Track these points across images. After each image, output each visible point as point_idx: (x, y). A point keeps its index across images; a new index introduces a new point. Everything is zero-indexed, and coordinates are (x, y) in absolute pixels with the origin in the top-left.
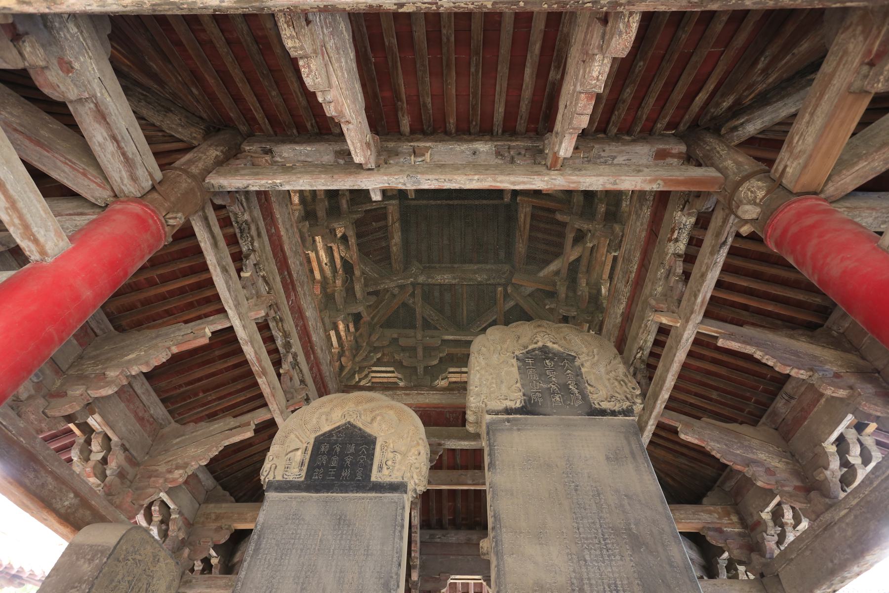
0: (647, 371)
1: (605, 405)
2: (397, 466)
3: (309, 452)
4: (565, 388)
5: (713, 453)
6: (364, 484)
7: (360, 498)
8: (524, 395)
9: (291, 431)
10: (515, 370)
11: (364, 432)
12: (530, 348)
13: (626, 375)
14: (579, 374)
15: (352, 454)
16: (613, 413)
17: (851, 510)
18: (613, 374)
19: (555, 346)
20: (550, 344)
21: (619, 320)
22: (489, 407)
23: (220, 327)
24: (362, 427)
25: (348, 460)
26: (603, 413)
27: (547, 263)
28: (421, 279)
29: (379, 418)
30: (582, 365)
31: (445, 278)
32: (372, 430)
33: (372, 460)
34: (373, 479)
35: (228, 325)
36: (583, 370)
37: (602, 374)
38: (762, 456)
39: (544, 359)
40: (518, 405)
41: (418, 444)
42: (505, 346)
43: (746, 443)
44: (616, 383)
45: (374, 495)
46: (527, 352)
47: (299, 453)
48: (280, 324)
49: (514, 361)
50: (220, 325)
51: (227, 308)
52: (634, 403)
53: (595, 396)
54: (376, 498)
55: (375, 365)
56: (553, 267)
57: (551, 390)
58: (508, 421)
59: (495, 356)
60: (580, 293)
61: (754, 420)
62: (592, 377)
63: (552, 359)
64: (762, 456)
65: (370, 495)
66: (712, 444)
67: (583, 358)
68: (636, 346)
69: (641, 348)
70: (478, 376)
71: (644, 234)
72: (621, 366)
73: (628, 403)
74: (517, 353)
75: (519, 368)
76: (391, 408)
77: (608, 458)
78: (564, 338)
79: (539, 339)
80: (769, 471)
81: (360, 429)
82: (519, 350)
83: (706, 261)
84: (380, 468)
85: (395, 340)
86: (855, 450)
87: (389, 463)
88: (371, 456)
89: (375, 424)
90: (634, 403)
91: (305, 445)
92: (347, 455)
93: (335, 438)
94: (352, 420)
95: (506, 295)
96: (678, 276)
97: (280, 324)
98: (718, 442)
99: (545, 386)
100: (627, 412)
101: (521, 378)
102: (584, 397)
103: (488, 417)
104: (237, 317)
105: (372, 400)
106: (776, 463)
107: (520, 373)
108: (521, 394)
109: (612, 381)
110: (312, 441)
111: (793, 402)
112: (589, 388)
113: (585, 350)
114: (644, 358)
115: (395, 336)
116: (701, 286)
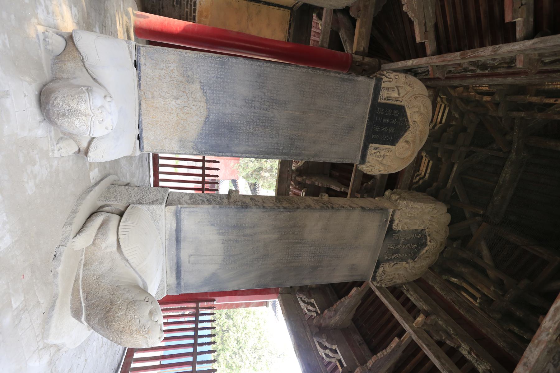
0: (395, 291)
1: (381, 269)
2: (375, 158)
3: (396, 103)
4: (397, 252)
5: (344, 298)
6: (369, 140)
7: (361, 138)
8: (399, 231)
9: (412, 88)
10: (416, 227)
11: (400, 138)
12: (428, 238)
13: (394, 282)
14: (403, 260)
15: (388, 131)
16: (375, 272)
17: (309, 341)
18: (397, 276)
19: (424, 251)
20: (427, 248)
21: (430, 283)
22: (397, 211)
23: (518, 29)
24: (405, 135)
25: (385, 129)
26: (377, 267)
27: (491, 249)
28: (513, 156)
29: (407, 146)
30: (408, 263)
31: (507, 174)
32: (401, 143)
33: (382, 144)
34: (371, 145)
35: (518, 35)
36: (404, 263)
37: (399, 271)
38: (337, 317)
39: (418, 244)
40: (394, 227)
41: (385, 170)
42: (434, 224)
43: (345, 314)
44: (391, 277)
45: (362, 145)
46: (425, 236)
47: (396, 95)
48: (505, 65)
49: (422, 228)
50: (520, 31)
51: (535, 40)
52: (378, 283)
53: (387, 266)
54: (360, 147)
55: (449, 112)
56: (485, 252)
57: (396, 243)
58: (386, 221)
59: (429, 217)
60: (458, 265)
61: (355, 320)
62: (399, 267)
63: (416, 248)
64: (337, 317)
65: (362, 143)
66: (348, 300)
67: (412, 264)
68: (410, 289)
69: (408, 290)
70: (419, 207)
71: (484, 331)
72: (401, 282)
73: (378, 280)
74: (427, 230)
75: (416, 230)
76: (412, 154)
77: (353, 265)
78: (428, 257)
79: (432, 243)
80: (330, 317)
81: (403, 135)
82: (429, 232)
83: (447, 365)
84: (376, 148)
85: (464, 129)
86: (331, 354)
87: (378, 154)
88: (385, 143)
89: (404, 144)
90: (378, 283)
91: (401, 100)
92: (388, 129)
93: (401, 119)
94: (410, 129)
95: (475, 215)
96: (445, 339)
97: (505, 65)
98: (348, 303)
99: (401, 242)
100: (374, 278)
101: (410, 230)
102: (388, 260)
103: (391, 210)
104: (523, 48)
105: (421, 140)
106: (333, 321)
107: (413, 230)
108: (400, 229)
109: (393, 276)
110: (402, 104)
111: (358, 344)
112: (393, 264)
113: (417, 266)
114: (402, 289)
115: (469, 131)
116: (432, 353)
